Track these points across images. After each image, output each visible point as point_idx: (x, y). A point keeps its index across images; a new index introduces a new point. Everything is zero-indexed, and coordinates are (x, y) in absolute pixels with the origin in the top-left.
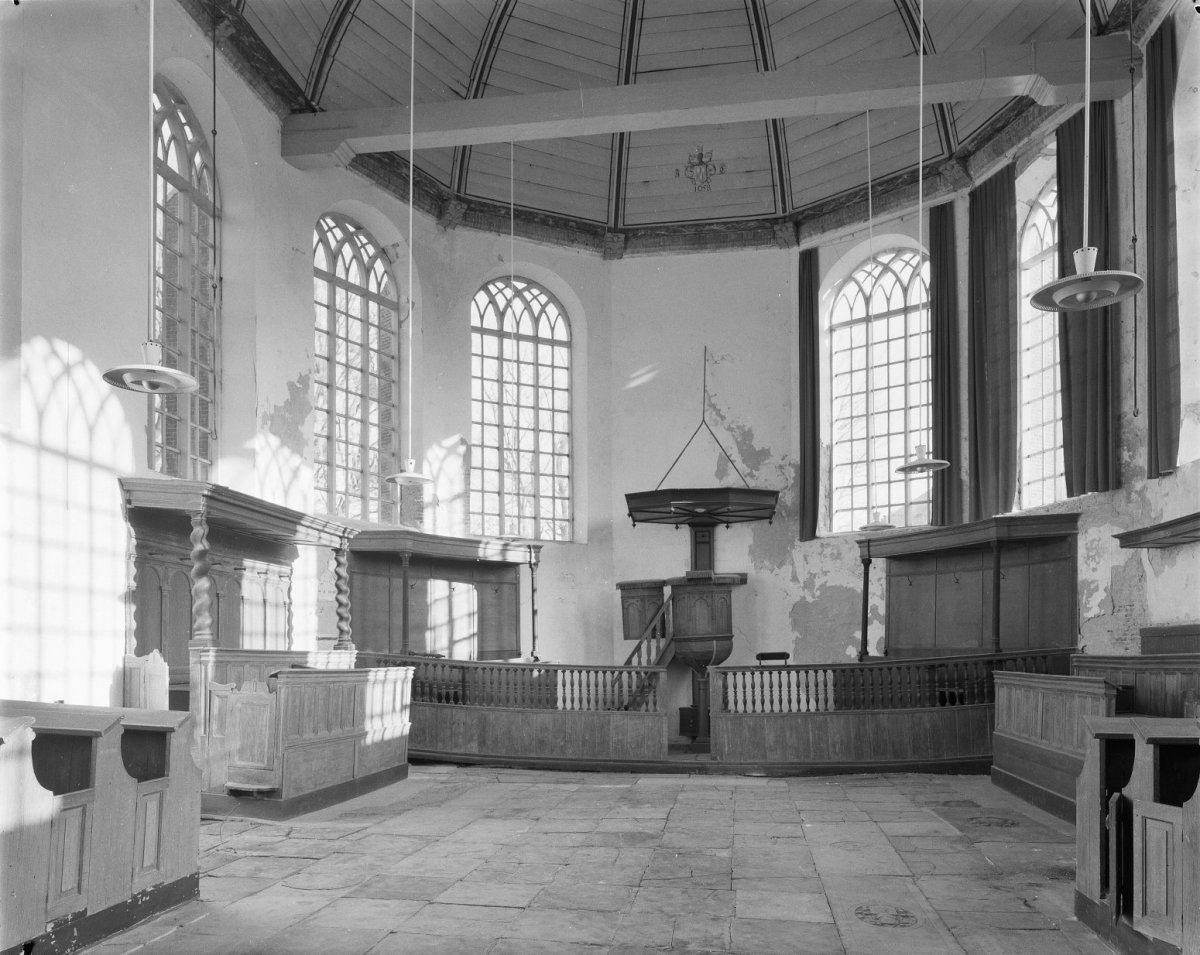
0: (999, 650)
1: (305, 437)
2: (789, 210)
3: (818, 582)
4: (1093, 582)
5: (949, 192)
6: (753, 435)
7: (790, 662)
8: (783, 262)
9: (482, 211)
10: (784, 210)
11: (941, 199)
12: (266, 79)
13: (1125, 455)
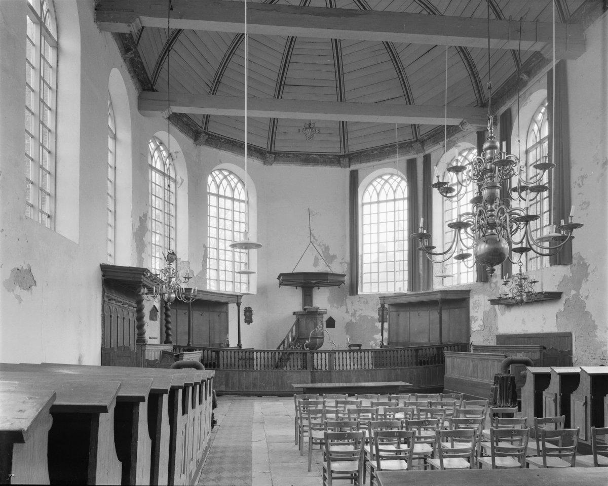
0: (442, 343)
3: (358, 314)
5: (414, 154)
6: (329, 248)
7: (362, 348)
10: (345, 152)
11: (411, 156)
12: (138, 76)
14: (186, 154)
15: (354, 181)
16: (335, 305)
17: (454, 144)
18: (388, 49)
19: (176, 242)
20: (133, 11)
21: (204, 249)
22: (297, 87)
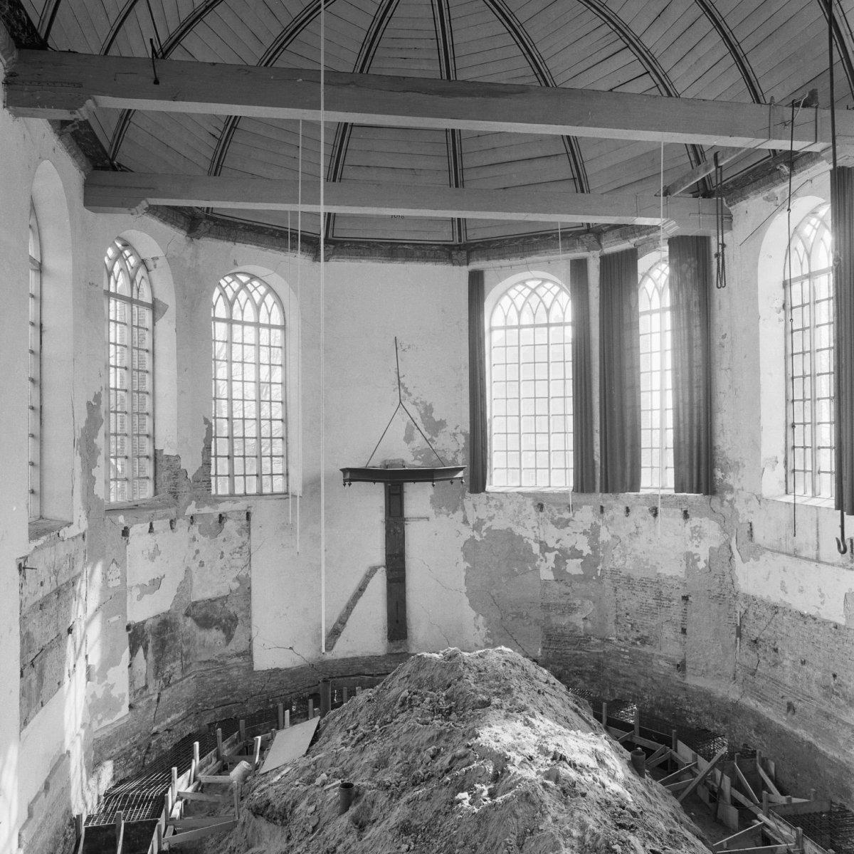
1: (98, 447)
2: (463, 239)
4: (696, 554)
5: (584, 251)
8: (458, 275)
9: (222, 226)
10: (460, 240)
11: (579, 254)
13: (719, 474)
14: (171, 260)
15: (476, 285)
16: (444, 509)
17: (655, 248)
18: (539, 76)
19: (154, 442)
20: (80, 86)
21: (207, 426)
22: (375, 129)
